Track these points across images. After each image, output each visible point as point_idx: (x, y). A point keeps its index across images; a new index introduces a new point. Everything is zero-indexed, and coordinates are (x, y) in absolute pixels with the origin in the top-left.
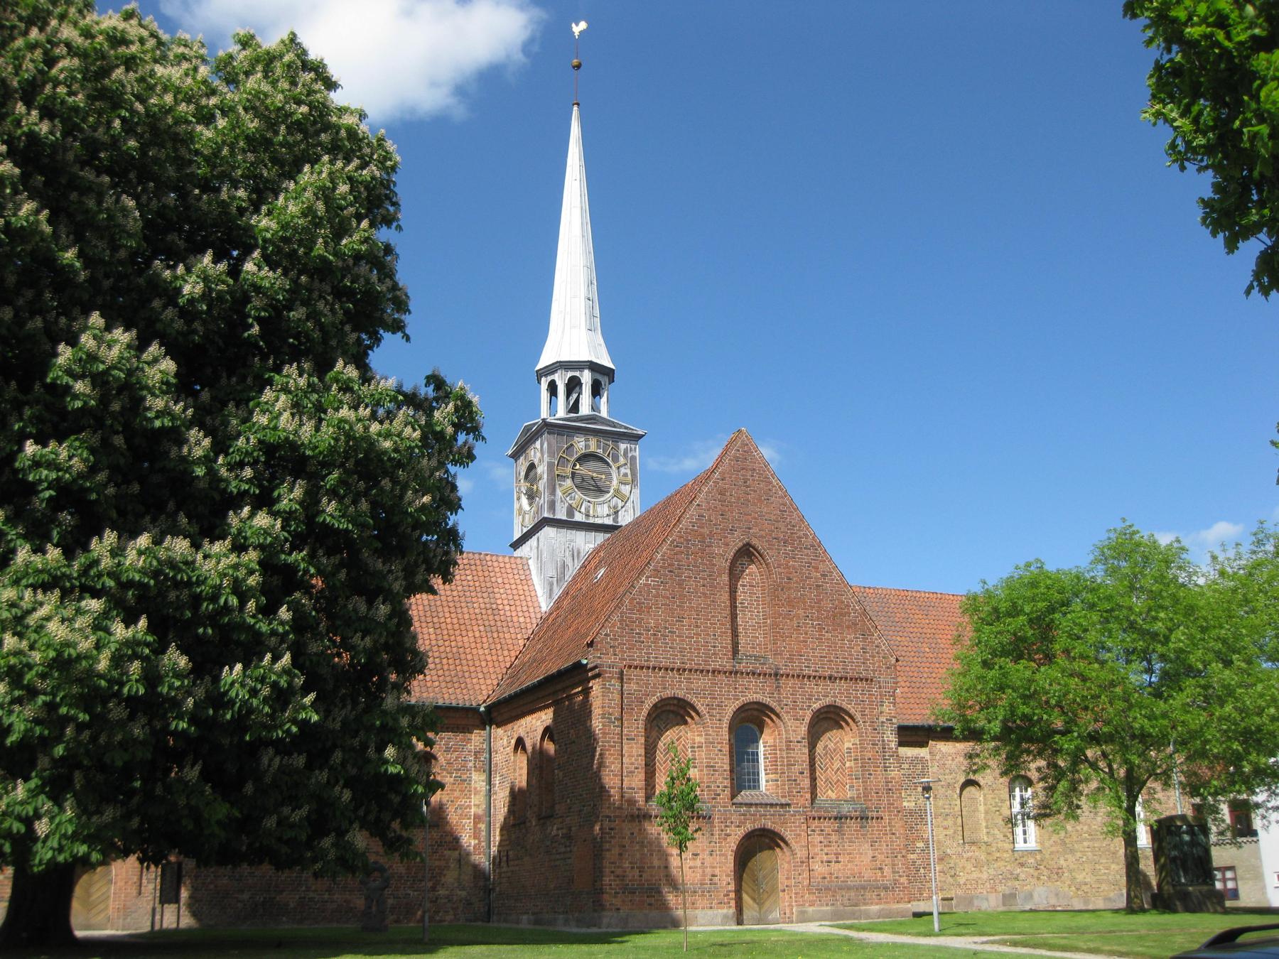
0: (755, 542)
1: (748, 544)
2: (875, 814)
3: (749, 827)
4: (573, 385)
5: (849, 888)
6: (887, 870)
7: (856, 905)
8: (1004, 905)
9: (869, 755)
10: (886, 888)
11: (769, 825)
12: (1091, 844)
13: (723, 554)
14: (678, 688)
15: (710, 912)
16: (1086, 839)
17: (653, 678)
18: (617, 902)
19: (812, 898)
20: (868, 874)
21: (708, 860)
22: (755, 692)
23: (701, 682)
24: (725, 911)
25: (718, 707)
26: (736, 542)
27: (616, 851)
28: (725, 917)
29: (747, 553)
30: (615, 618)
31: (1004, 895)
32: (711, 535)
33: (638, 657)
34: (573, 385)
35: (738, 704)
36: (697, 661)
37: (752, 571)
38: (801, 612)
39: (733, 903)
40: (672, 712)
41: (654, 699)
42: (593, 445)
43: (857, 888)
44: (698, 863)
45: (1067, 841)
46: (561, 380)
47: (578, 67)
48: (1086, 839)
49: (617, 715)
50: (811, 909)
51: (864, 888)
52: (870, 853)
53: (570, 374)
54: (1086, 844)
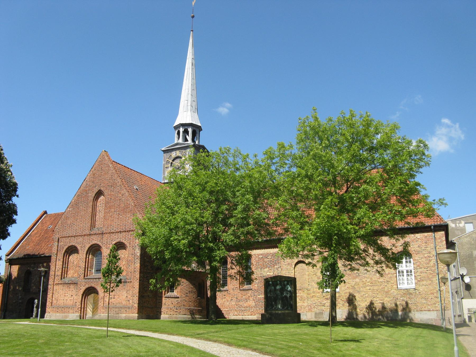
0: (102, 189)
1: (100, 190)
2: (129, 281)
3: (87, 286)
4: (186, 132)
5: (116, 308)
6: (131, 301)
7: (118, 314)
8: (315, 317)
9: (130, 259)
10: (129, 308)
11: (93, 285)
12: (372, 288)
13: (92, 195)
14: (73, 242)
15: (73, 314)
16: (368, 286)
17: (68, 240)
18: (49, 310)
19: (103, 311)
20: (124, 303)
21: (75, 297)
22: (95, 240)
23: (81, 239)
24: (77, 314)
25: (83, 248)
26: (96, 190)
27: (51, 295)
28: (77, 316)
29: (99, 193)
30: (60, 222)
31: (316, 314)
32: (89, 190)
33: (65, 234)
34: (186, 132)
35: (90, 245)
36: (79, 233)
37: (102, 198)
38: (113, 210)
39: (80, 311)
40: (72, 250)
41: (67, 247)
42: (178, 153)
43: (118, 308)
44: (72, 298)
45: (356, 287)
46: (181, 130)
47: (193, 17)
48: (368, 286)
49: (56, 253)
50: (102, 315)
51: (121, 308)
52: (126, 295)
53: (195, 128)
54: (368, 288)
